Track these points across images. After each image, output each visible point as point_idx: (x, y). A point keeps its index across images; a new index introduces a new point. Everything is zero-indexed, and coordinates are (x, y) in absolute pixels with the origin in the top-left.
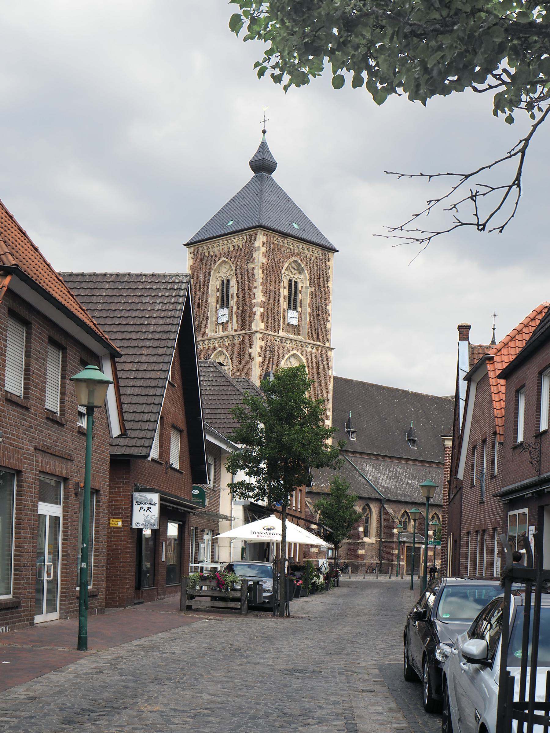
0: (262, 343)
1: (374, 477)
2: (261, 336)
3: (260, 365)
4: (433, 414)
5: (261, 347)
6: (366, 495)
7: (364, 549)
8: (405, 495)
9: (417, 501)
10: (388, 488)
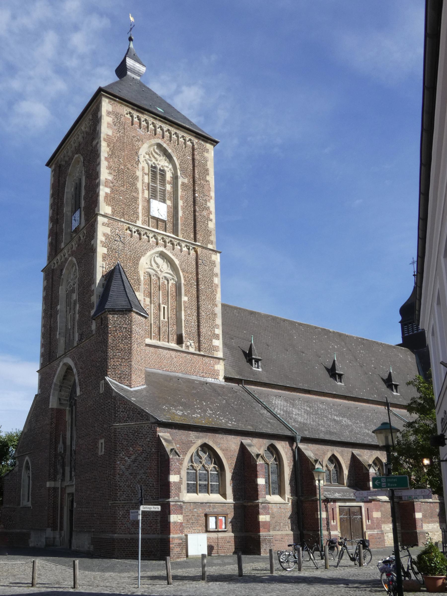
0: (108, 230)
1: (286, 411)
2: (106, 220)
3: (104, 258)
4: (360, 353)
5: (104, 235)
6: (269, 431)
7: (268, 513)
8: (331, 433)
9: (349, 440)
10: (304, 424)
